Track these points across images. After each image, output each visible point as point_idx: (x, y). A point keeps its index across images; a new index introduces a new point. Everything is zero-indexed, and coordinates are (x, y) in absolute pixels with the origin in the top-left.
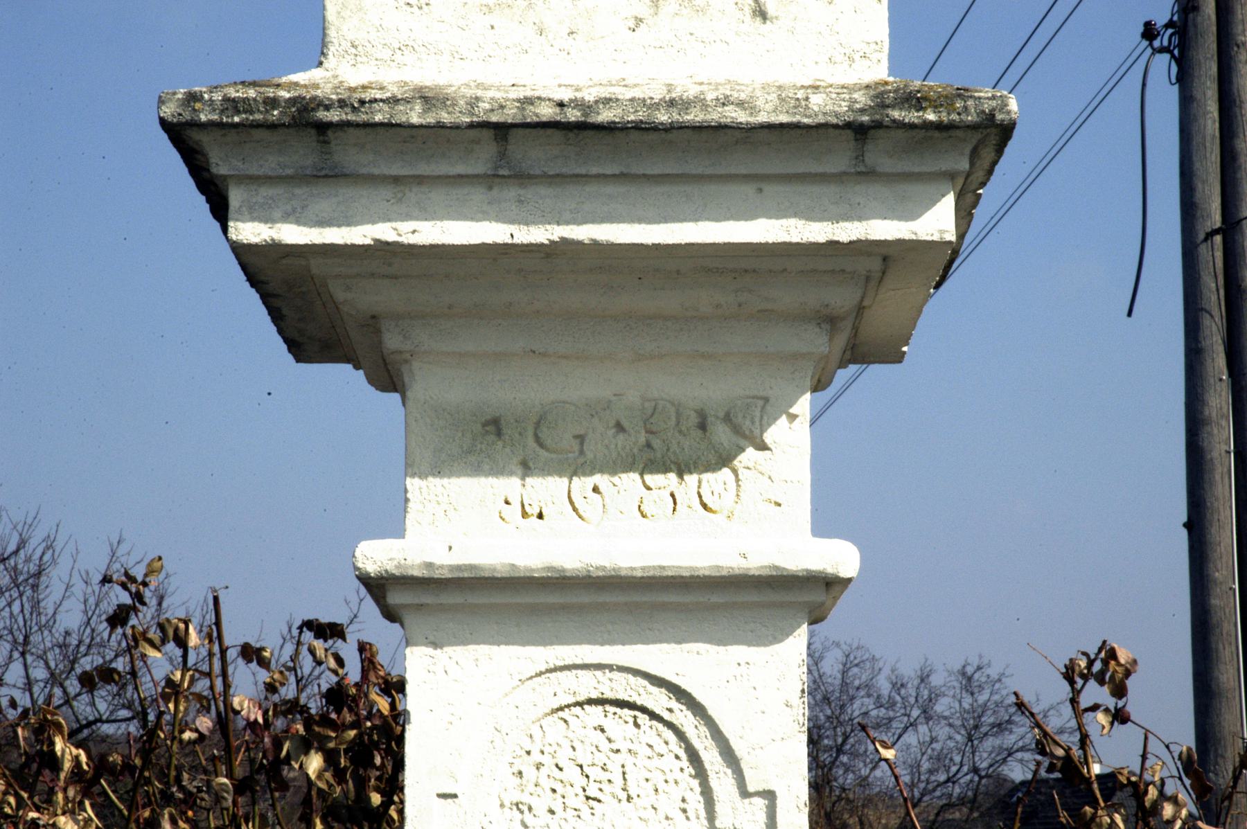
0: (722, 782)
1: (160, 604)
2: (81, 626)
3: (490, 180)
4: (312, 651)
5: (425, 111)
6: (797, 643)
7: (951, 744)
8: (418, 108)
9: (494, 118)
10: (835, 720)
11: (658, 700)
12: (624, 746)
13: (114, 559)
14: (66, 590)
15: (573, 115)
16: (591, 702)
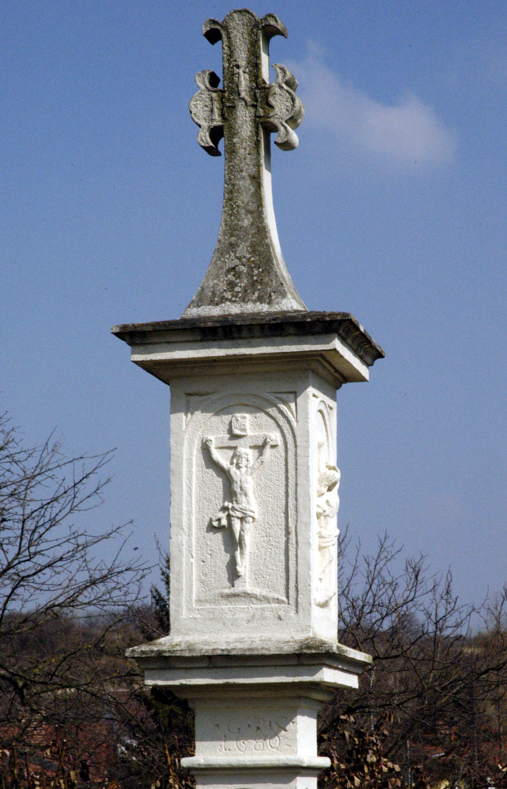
1: (416, 577)
2: (363, 595)
3: (208, 668)
5: (189, 653)
8: (188, 652)
9: (206, 654)
13: (383, 549)
14: (354, 570)
15: (225, 653)
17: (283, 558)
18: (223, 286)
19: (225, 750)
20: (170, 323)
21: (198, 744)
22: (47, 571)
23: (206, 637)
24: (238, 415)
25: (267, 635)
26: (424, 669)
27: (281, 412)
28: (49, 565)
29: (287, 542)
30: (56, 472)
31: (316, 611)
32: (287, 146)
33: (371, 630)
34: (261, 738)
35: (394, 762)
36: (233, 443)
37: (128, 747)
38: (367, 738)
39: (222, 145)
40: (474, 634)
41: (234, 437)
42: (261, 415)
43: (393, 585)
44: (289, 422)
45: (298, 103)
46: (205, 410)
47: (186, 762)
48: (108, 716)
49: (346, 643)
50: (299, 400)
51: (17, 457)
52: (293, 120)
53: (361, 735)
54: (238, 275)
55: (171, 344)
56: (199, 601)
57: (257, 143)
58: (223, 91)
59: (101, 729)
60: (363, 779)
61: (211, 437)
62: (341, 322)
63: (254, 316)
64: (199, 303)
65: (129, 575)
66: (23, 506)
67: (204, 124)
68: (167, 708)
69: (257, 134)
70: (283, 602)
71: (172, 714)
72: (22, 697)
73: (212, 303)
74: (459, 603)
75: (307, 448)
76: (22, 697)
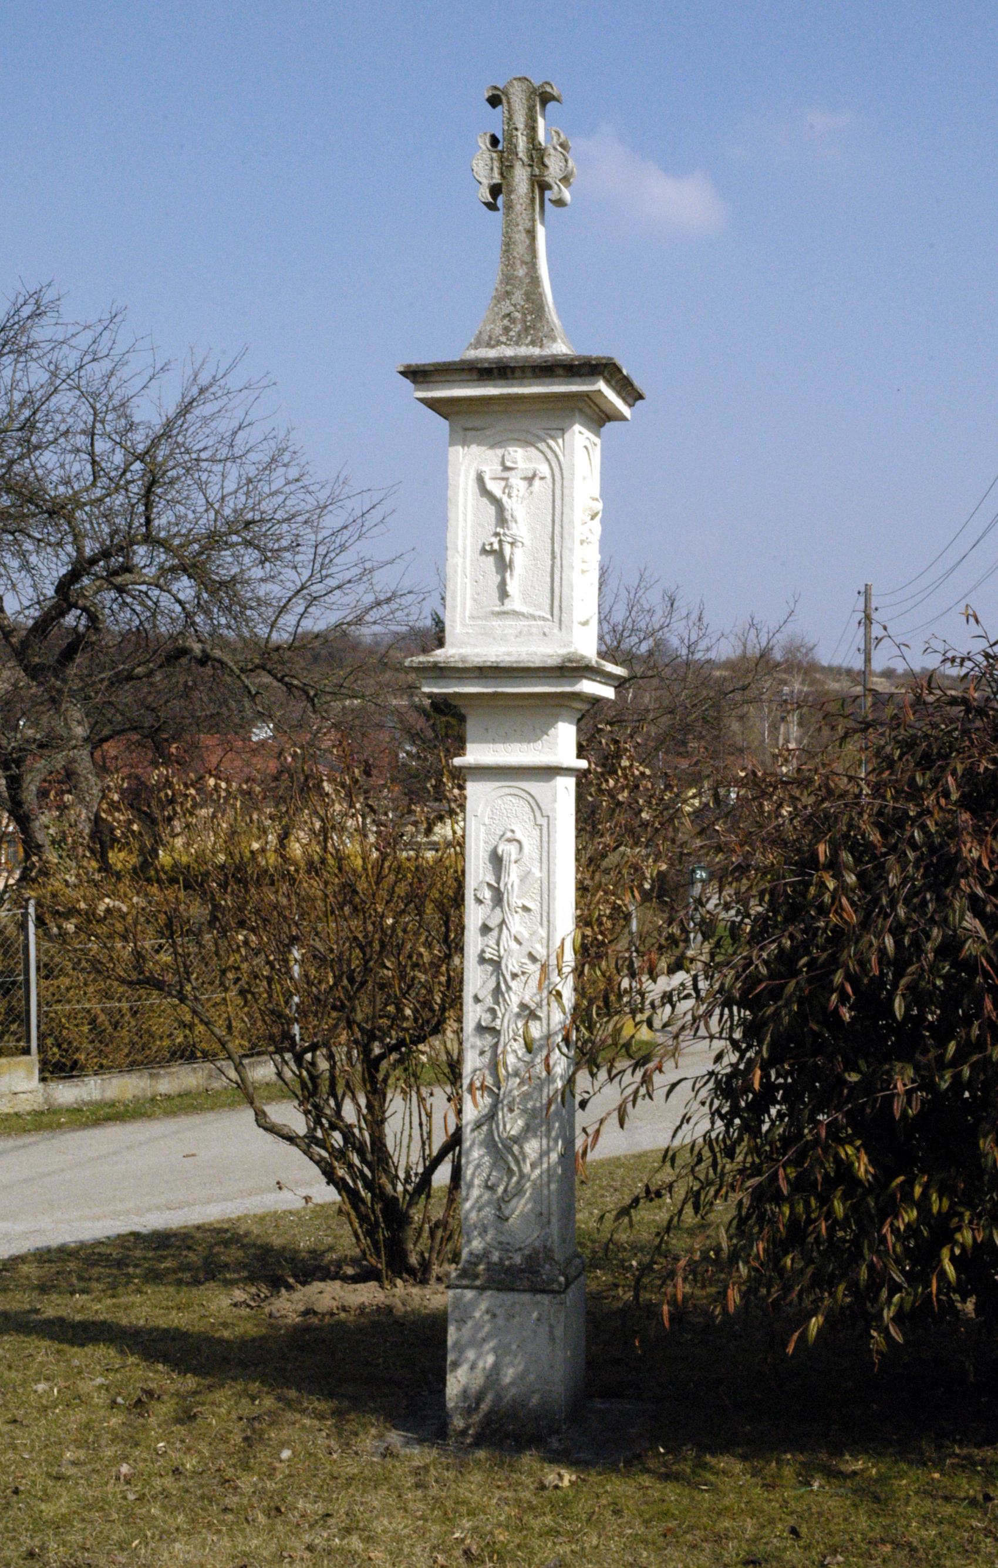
11: (524, 795)
17: (548, 580)
18: (498, 331)
20: (450, 364)
21: (469, 746)
22: (336, 592)
23: (477, 650)
24: (511, 449)
25: (533, 649)
26: (676, 689)
27: (550, 447)
28: (339, 587)
29: (553, 566)
30: (347, 502)
31: (577, 628)
32: (560, 203)
33: (629, 652)
35: (646, 767)
36: (505, 474)
37: (407, 753)
38: (622, 745)
39: (500, 201)
40: (723, 658)
41: (507, 469)
42: (532, 450)
43: (651, 612)
44: (557, 456)
45: (571, 163)
46: (479, 444)
47: (457, 761)
48: (391, 725)
49: (603, 658)
50: (566, 436)
51: (311, 488)
52: (566, 179)
53: (616, 742)
54: (513, 321)
55: (450, 383)
56: (472, 617)
57: (533, 199)
58: (502, 152)
59: (384, 737)
60: (617, 781)
61: (484, 468)
62: (606, 365)
63: (526, 358)
64: (477, 345)
65: (410, 598)
66: (316, 533)
67: (485, 181)
68: (444, 719)
69: (533, 191)
70: (547, 620)
71: (448, 726)
72: (313, 705)
73: (489, 345)
74: (710, 630)
75: (572, 480)
76: (313, 705)
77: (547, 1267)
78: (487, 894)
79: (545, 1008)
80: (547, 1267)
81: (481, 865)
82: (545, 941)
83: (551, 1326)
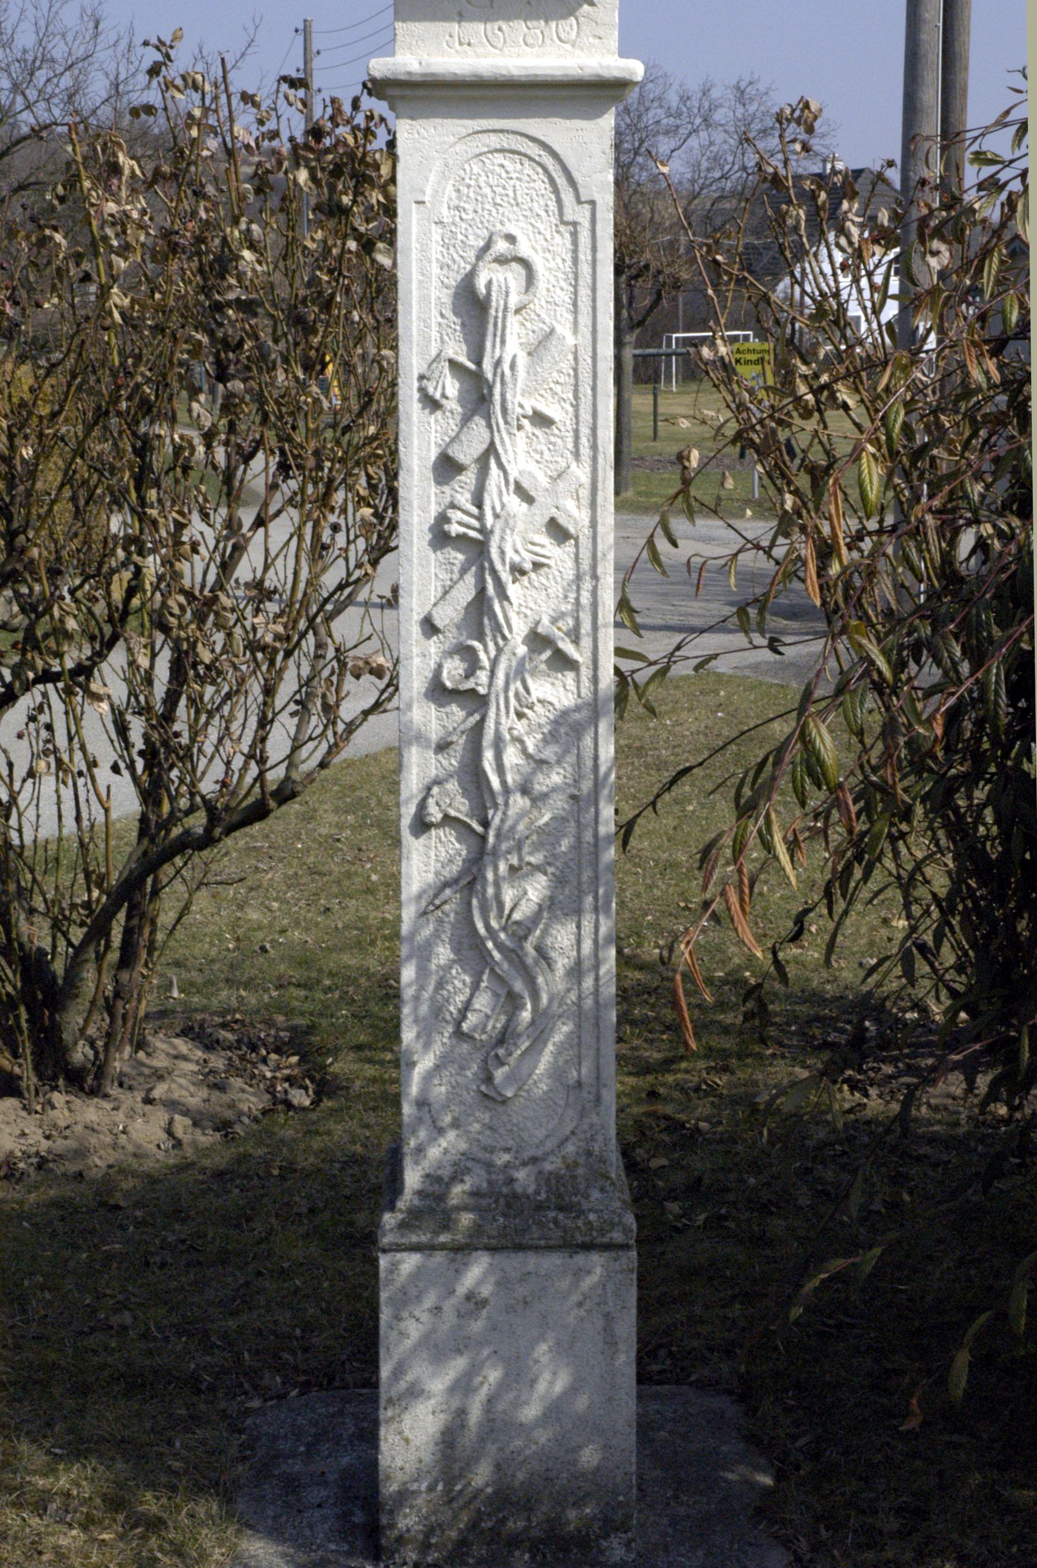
0: (568, 196)
4: (286, 97)
6: (608, 121)
7: (726, 147)
10: (634, 128)
11: (534, 150)
12: (514, 175)
16: (497, 151)
19: (461, 44)
34: (538, 18)
77: (595, 1194)
78: (452, 387)
79: (586, 642)
80: (595, 1194)
81: (435, 318)
82: (585, 493)
83: (607, 1316)
